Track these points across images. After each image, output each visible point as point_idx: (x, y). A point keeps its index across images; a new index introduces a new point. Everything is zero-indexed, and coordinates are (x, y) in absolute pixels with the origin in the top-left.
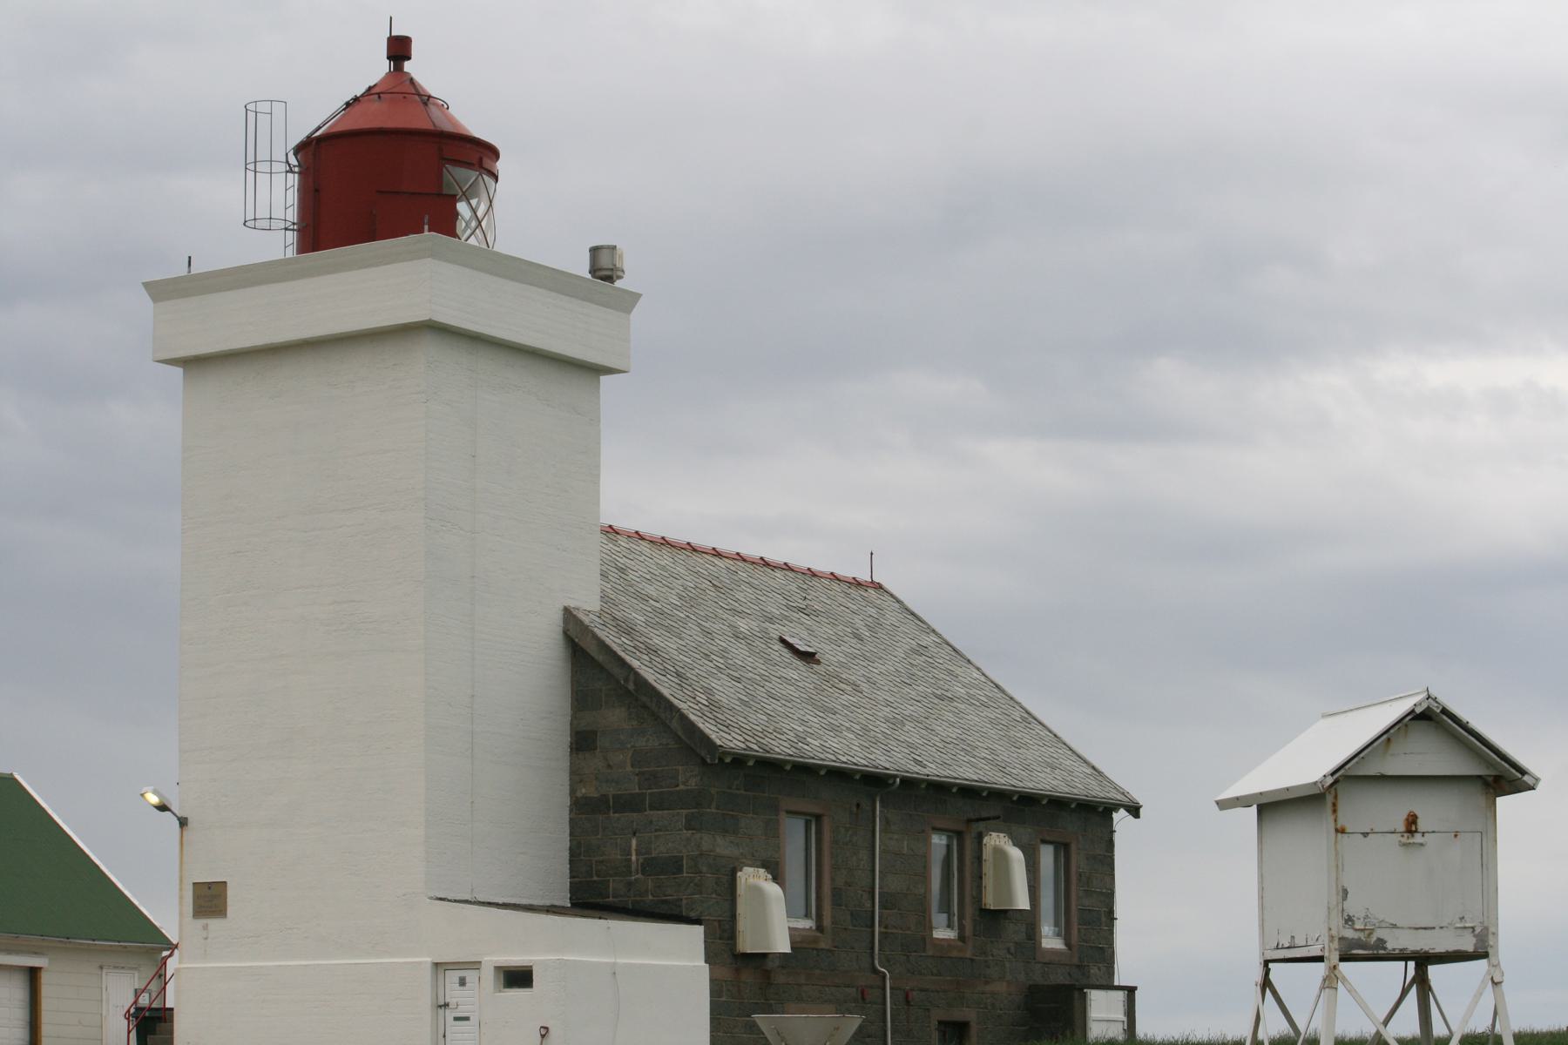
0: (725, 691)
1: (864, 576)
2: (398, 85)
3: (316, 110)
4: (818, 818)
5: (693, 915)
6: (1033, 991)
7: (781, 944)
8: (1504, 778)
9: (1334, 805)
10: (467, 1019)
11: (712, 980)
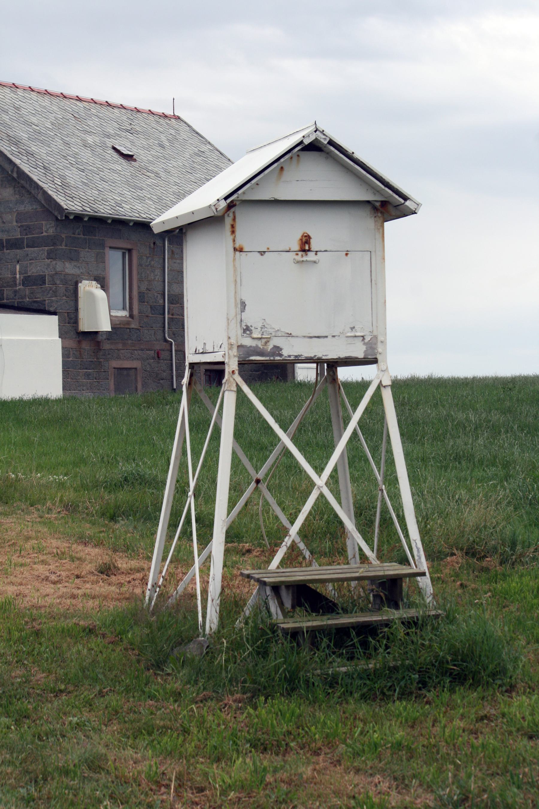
0: (73, 177)
1: (169, 112)
4: (130, 251)
5: (52, 309)
7: (105, 326)
8: (389, 205)
9: (233, 226)
11: (63, 348)
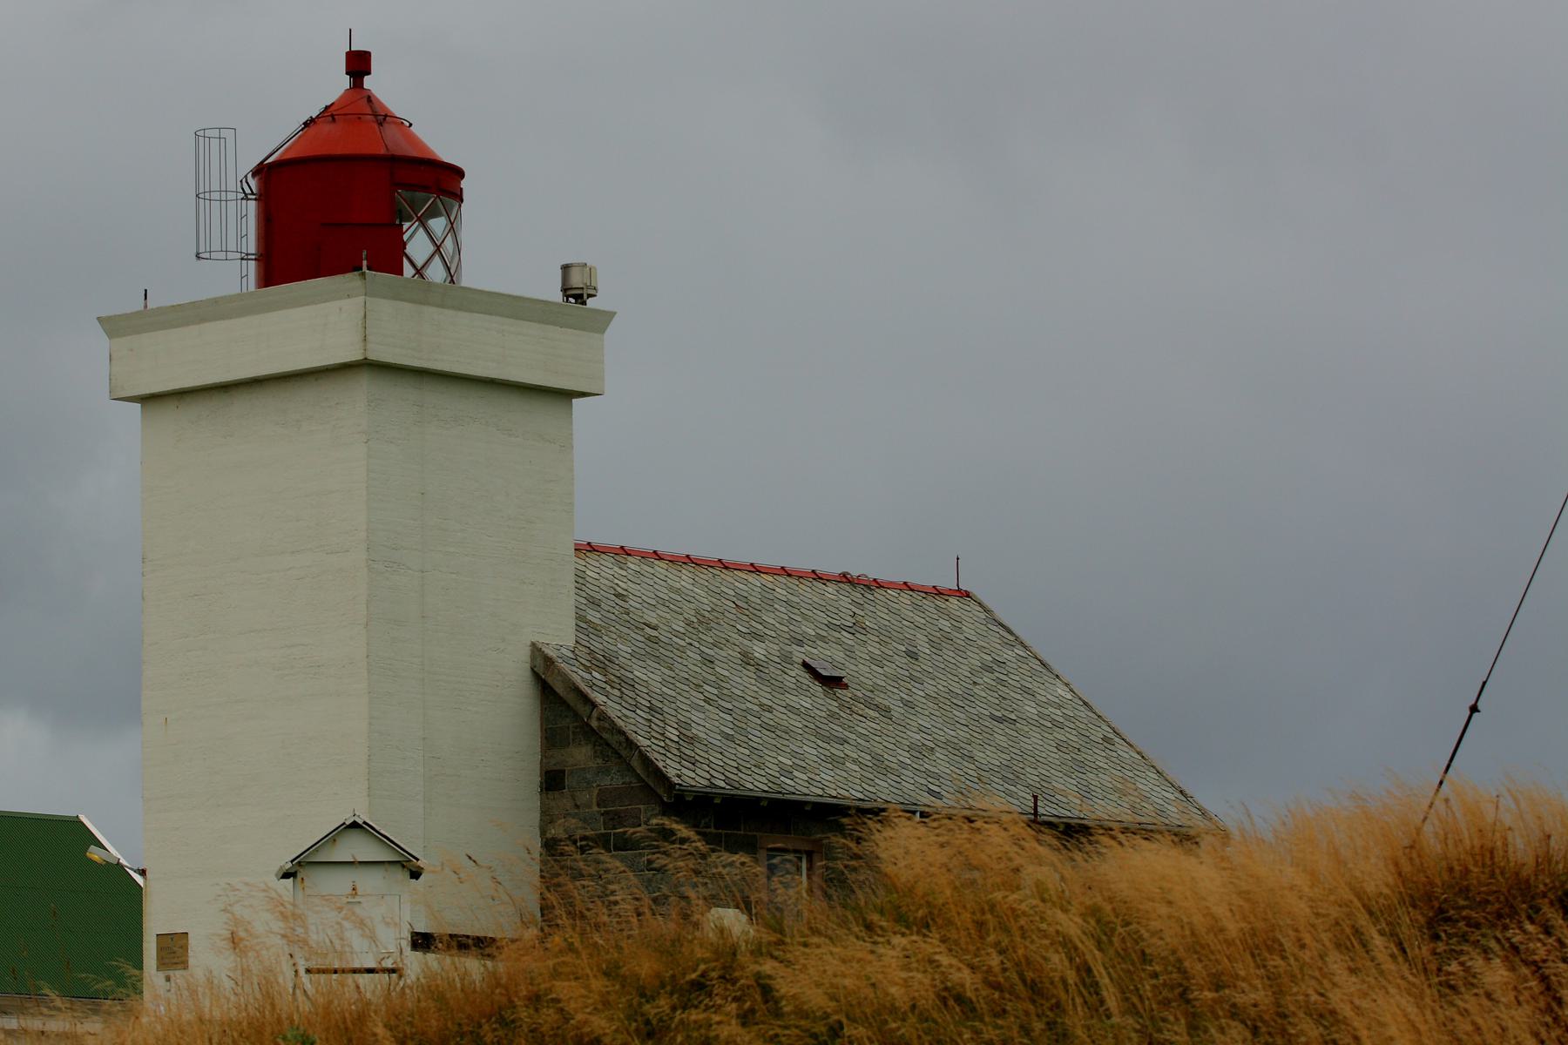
0: (706, 724)
2: (358, 107)
3: (271, 131)
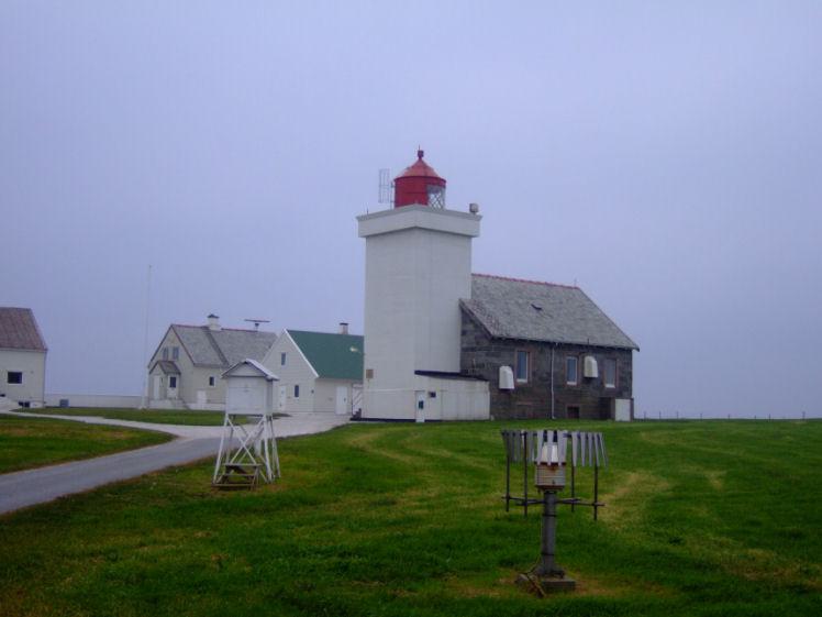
1: (572, 285)
2: (421, 164)
3: (399, 170)
6: (602, 399)
10: (283, 363)
